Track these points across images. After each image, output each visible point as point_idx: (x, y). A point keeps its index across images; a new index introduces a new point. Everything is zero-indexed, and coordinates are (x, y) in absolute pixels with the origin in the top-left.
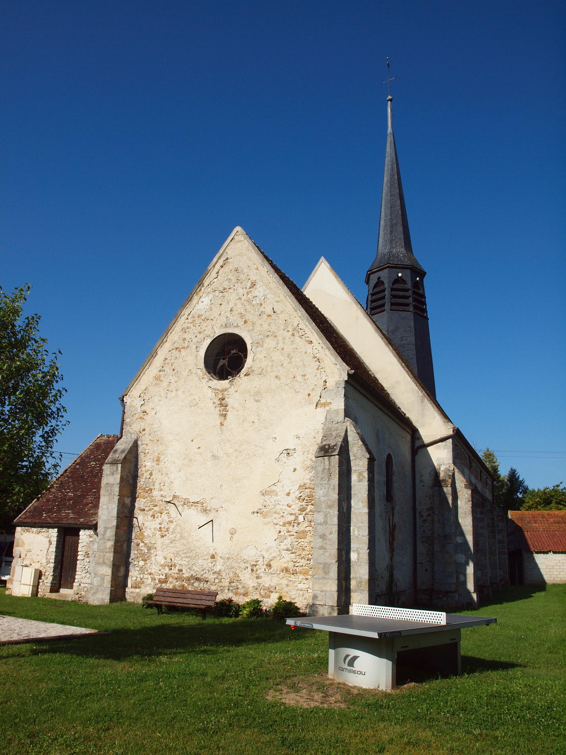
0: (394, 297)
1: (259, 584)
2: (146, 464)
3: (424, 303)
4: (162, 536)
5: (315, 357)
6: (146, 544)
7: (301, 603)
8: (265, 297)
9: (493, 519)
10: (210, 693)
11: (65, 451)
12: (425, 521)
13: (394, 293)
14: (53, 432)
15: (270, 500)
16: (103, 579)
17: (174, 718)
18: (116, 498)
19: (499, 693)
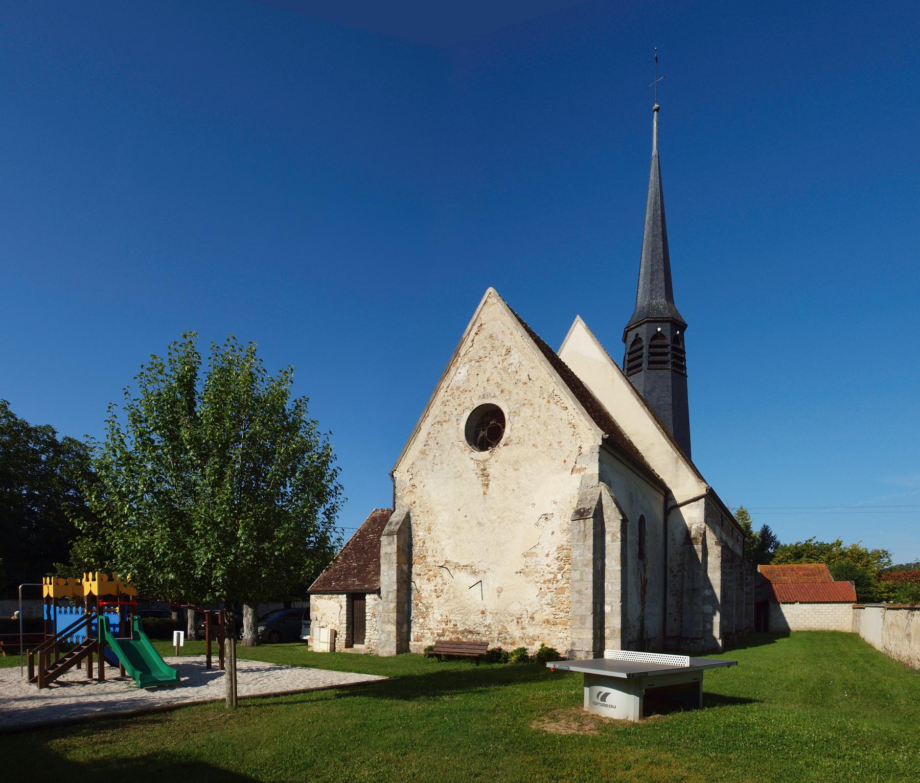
0: (652, 354)
2: (419, 533)
3: (684, 359)
4: (438, 597)
5: (570, 423)
6: (424, 604)
7: (561, 649)
8: (520, 364)
9: (742, 573)
11: (346, 525)
12: (675, 576)
13: (652, 350)
14: (333, 508)
15: (531, 561)
16: (389, 635)
17: (458, 745)
18: (395, 565)
19: (735, 724)
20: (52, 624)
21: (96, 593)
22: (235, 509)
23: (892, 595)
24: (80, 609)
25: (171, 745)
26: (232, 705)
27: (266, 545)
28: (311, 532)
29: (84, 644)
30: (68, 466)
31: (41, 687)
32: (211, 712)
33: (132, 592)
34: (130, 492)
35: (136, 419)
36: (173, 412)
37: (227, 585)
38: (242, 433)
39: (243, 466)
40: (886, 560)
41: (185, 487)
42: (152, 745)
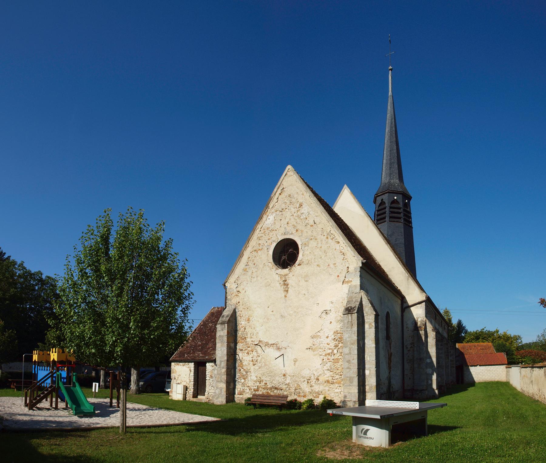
0: (392, 212)
1: (312, 390)
2: (242, 323)
3: (410, 218)
4: (254, 365)
6: (244, 370)
7: (337, 400)
9: (448, 348)
10: (284, 453)
11: (194, 318)
14: (187, 307)
15: (317, 341)
16: (221, 390)
18: (226, 344)
19: (447, 443)
20: (36, 375)
21: (56, 360)
22: (128, 310)
23: (524, 360)
24: (48, 368)
25: (89, 452)
26: (123, 431)
27: (146, 331)
28: (173, 323)
29: (50, 387)
30: (47, 291)
31: (30, 409)
32: (111, 434)
33: (73, 359)
34: (75, 303)
35: (79, 262)
36: (98, 256)
37: (123, 356)
38: (134, 264)
39: (134, 283)
40: (520, 341)
41: (102, 299)
42: (79, 451)
